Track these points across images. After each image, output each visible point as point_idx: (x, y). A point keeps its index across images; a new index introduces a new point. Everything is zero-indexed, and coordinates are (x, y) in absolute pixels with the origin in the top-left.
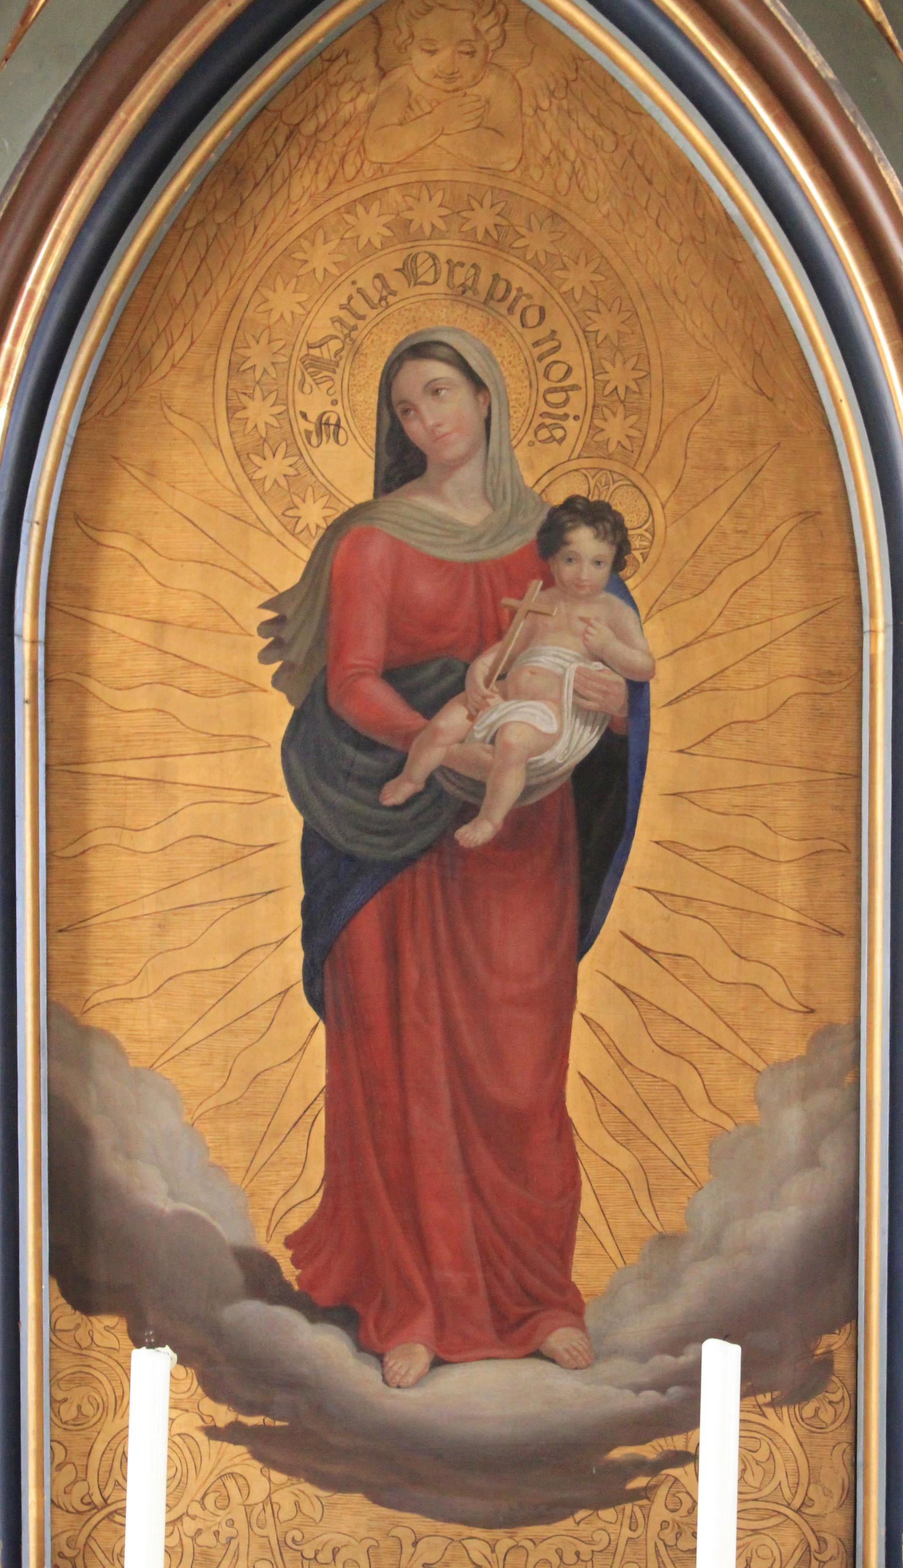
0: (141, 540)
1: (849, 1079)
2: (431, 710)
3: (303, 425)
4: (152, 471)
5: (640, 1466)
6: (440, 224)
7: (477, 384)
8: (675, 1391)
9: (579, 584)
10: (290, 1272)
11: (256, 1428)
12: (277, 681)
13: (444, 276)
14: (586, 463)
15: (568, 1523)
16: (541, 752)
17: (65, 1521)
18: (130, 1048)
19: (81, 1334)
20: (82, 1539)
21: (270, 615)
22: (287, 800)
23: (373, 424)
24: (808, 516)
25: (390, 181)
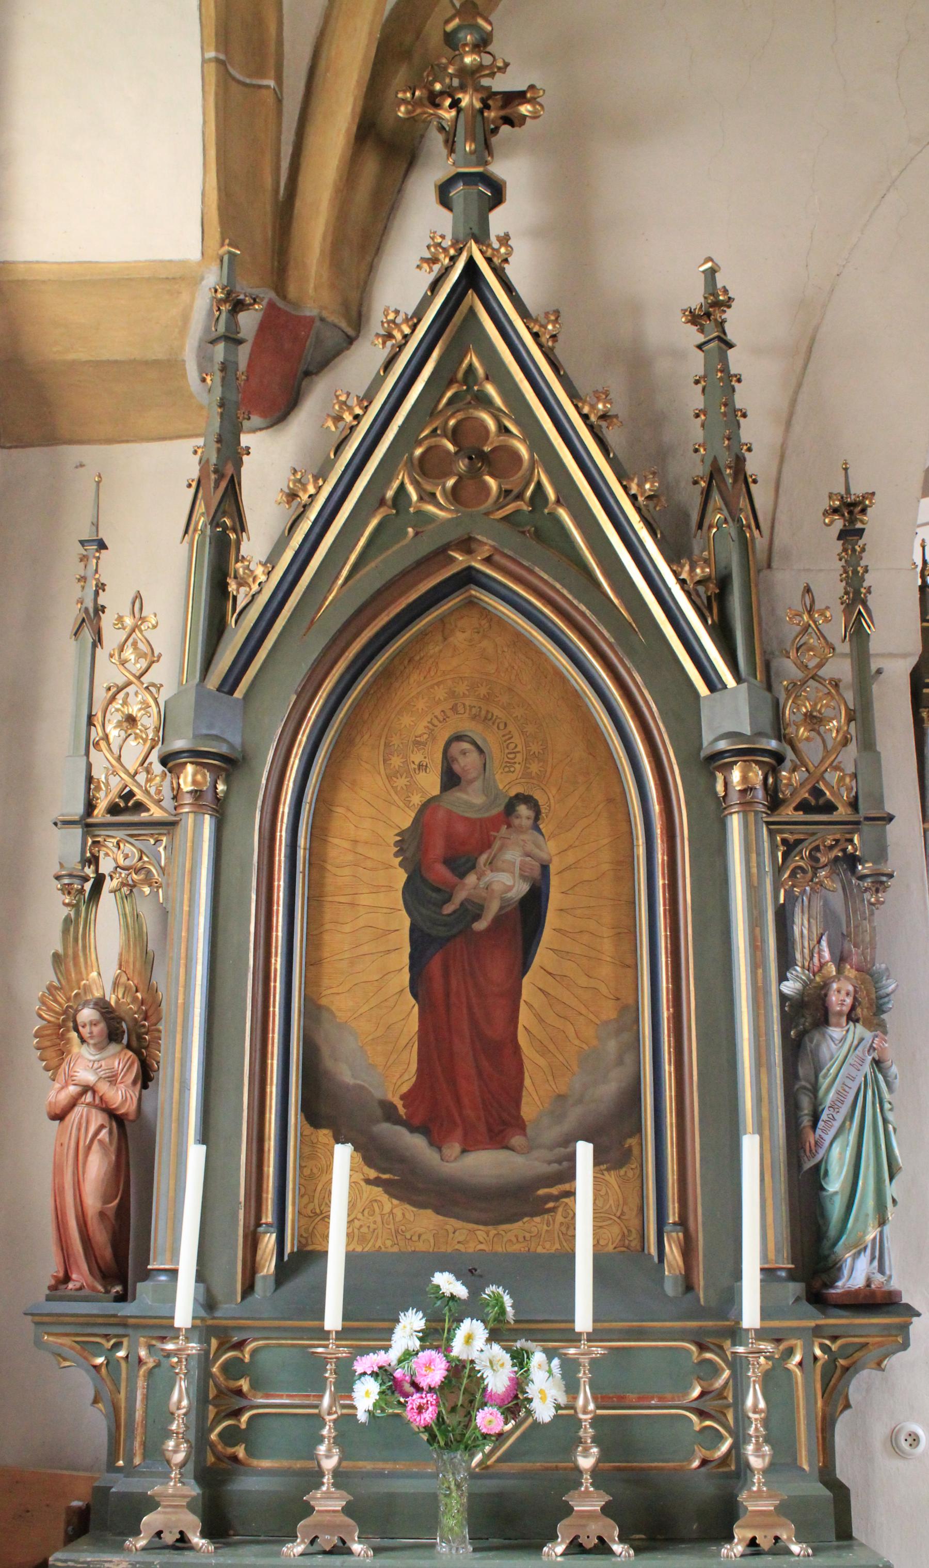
0: (348, 809)
1: (635, 1028)
2: (462, 875)
3: (413, 766)
4: (354, 783)
5: (550, 1198)
6: (467, 693)
7: (480, 751)
8: (565, 1164)
9: (521, 826)
10: (402, 1111)
11: (387, 1180)
12: (401, 865)
13: (468, 711)
14: (523, 780)
15: (520, 1223)
16: (506, 893)
17: (304, 1221)
18: (338, 1014)
19: (313, 1137)
20: (311, 1228)
21: (398, 838)
22: (404, 912)
23: (440, 766)
24: (610, 801)
25: (448, 677)
